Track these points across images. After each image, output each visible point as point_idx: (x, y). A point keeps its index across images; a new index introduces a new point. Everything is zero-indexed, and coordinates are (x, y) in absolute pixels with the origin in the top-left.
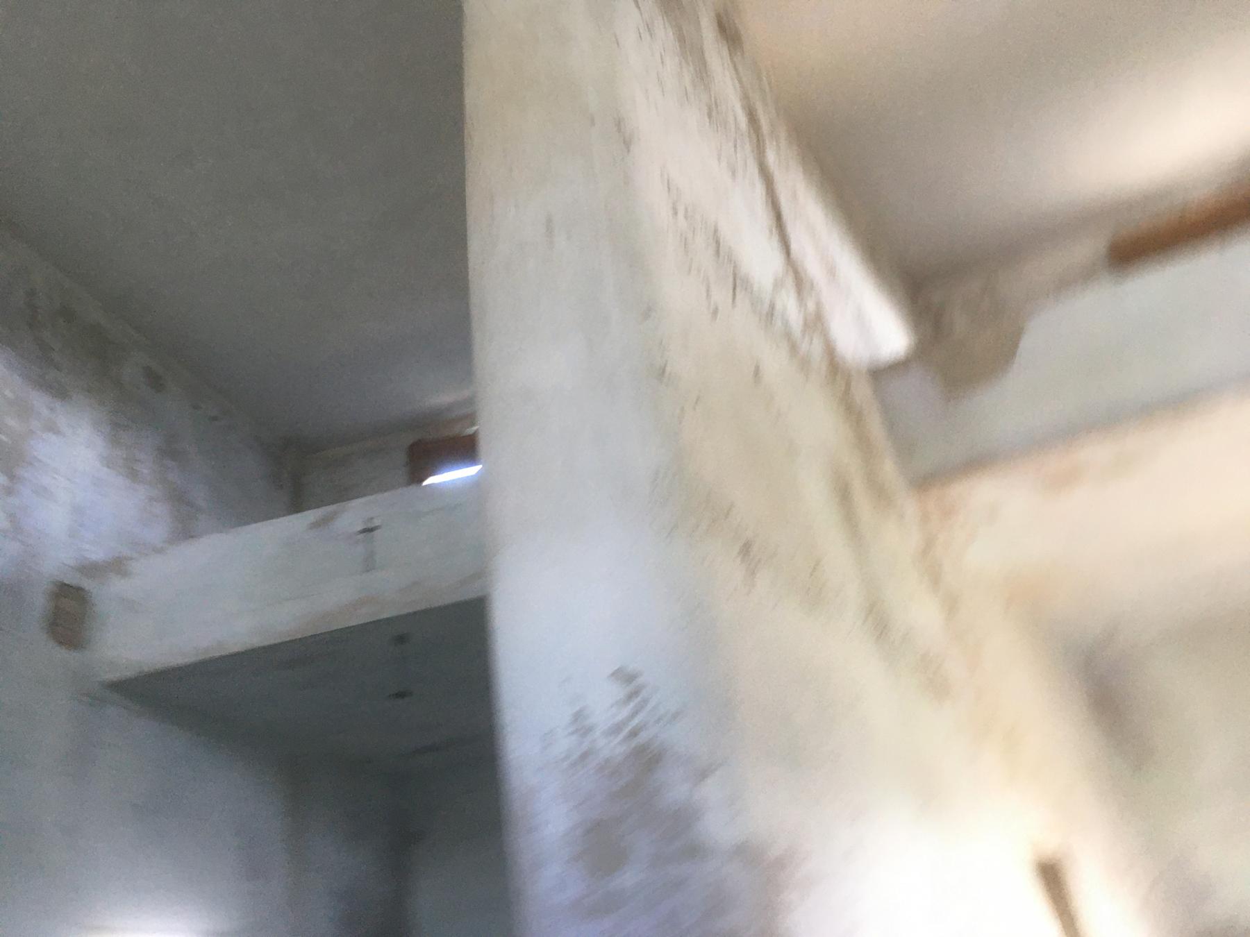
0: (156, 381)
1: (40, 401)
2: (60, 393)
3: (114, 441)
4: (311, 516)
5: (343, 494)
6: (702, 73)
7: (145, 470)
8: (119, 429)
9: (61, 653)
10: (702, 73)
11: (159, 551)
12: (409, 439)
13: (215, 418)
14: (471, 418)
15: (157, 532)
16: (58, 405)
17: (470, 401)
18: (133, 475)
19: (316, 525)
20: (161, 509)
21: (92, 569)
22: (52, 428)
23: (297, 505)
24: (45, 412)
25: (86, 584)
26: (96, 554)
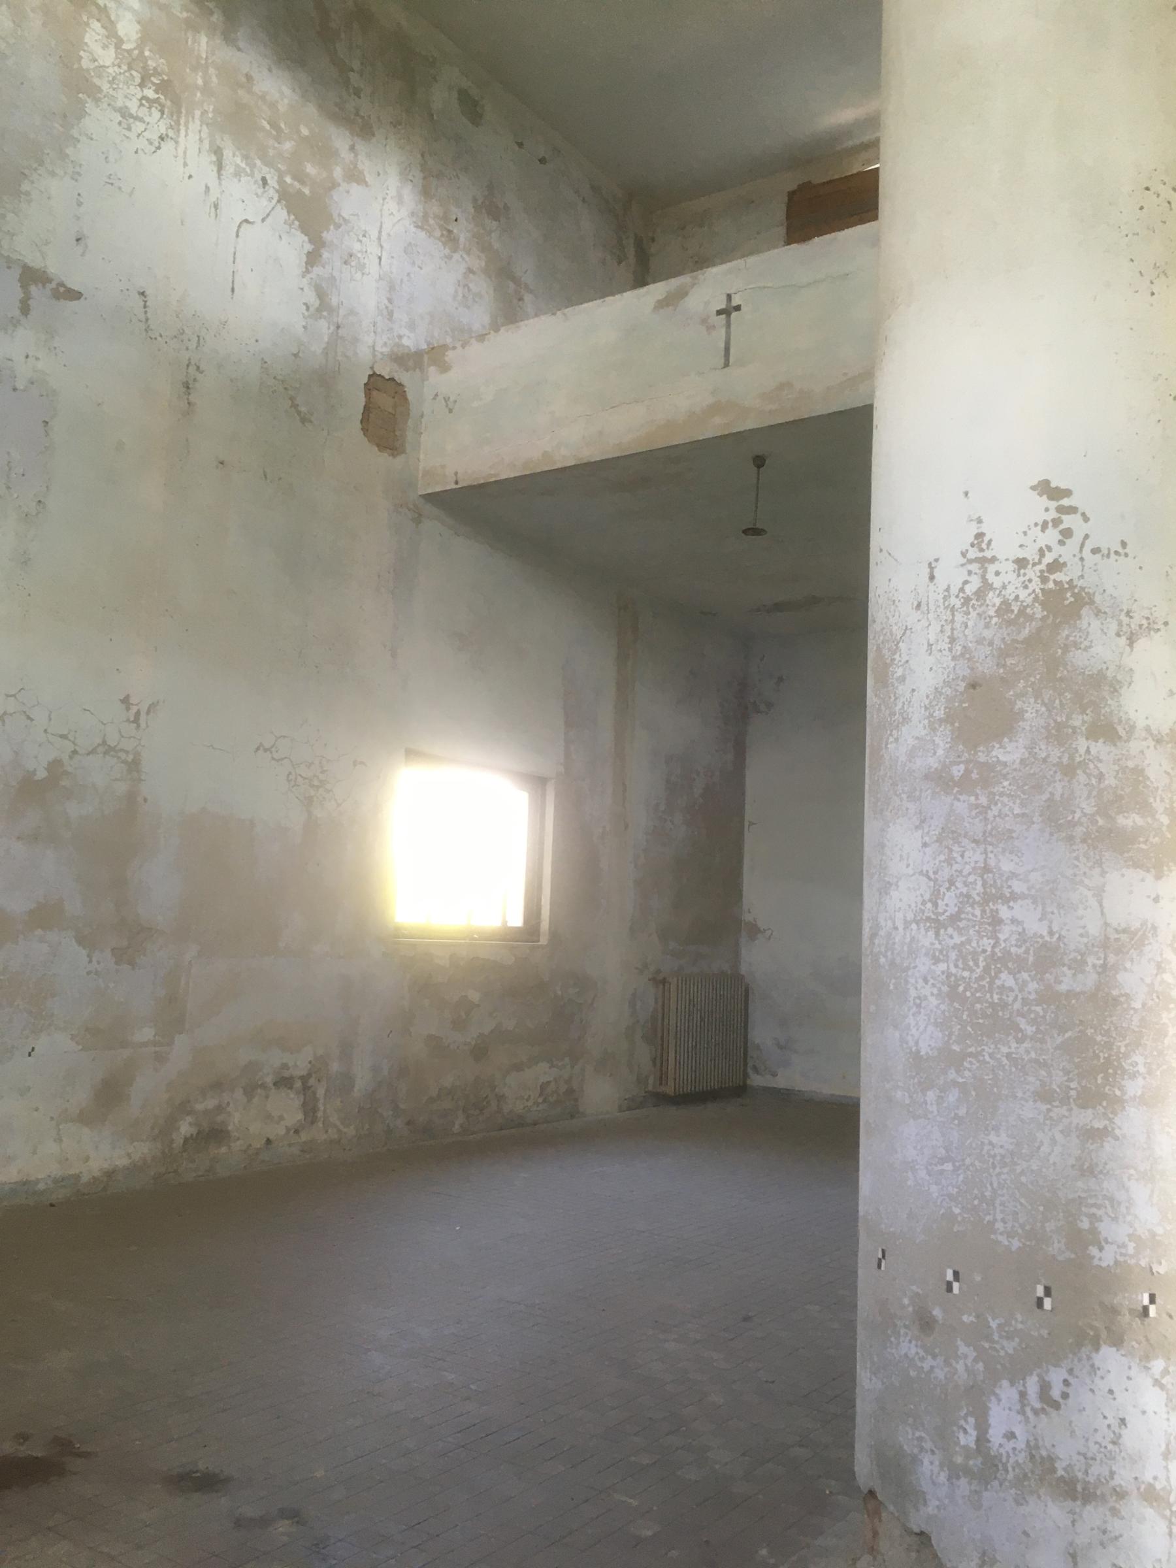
0: (471, 108)
1: (341, 140)
2: (364, 129)
3: (426, 193)
4: (657, 290)
5: (701, 262)
6: (500, 940)
7: (463, 229)
8: (237, 153)
9: (383, 458)
10: (500, 940)
11: (481, 338)
12: (790, 181)
13: (542, 161)
14: (873, 146)
15: (479, 316)
16: (361, 146)
17: (873, 122)
18: (450, 239)
19: (662, 304)
20: (482, 286)
21: (412, 360)
22: (354, 176)
23: (641, 280)
24: (346, 155)
25: (403, 377)
26: (411, 341)
